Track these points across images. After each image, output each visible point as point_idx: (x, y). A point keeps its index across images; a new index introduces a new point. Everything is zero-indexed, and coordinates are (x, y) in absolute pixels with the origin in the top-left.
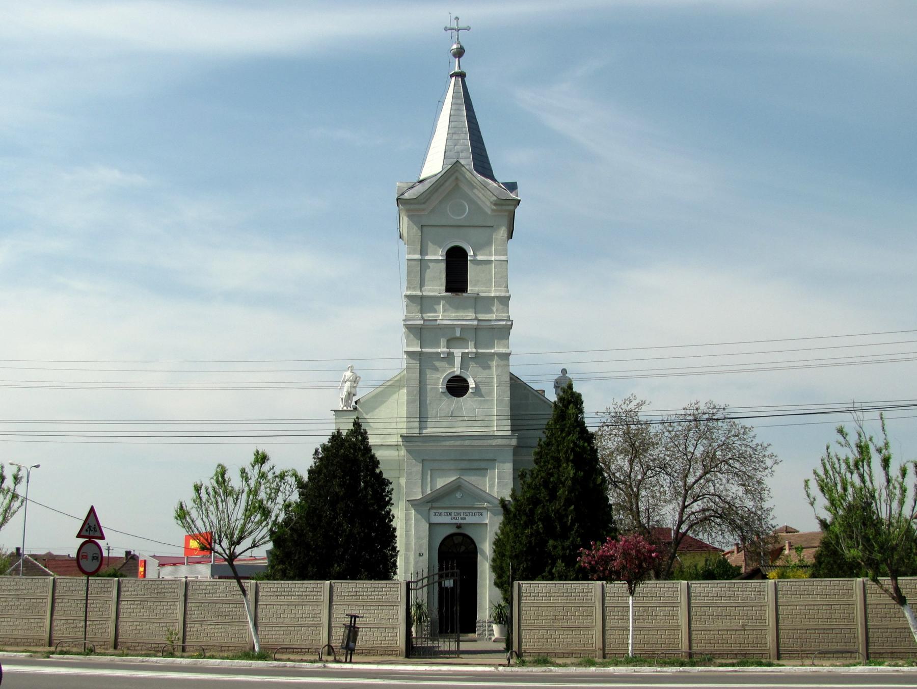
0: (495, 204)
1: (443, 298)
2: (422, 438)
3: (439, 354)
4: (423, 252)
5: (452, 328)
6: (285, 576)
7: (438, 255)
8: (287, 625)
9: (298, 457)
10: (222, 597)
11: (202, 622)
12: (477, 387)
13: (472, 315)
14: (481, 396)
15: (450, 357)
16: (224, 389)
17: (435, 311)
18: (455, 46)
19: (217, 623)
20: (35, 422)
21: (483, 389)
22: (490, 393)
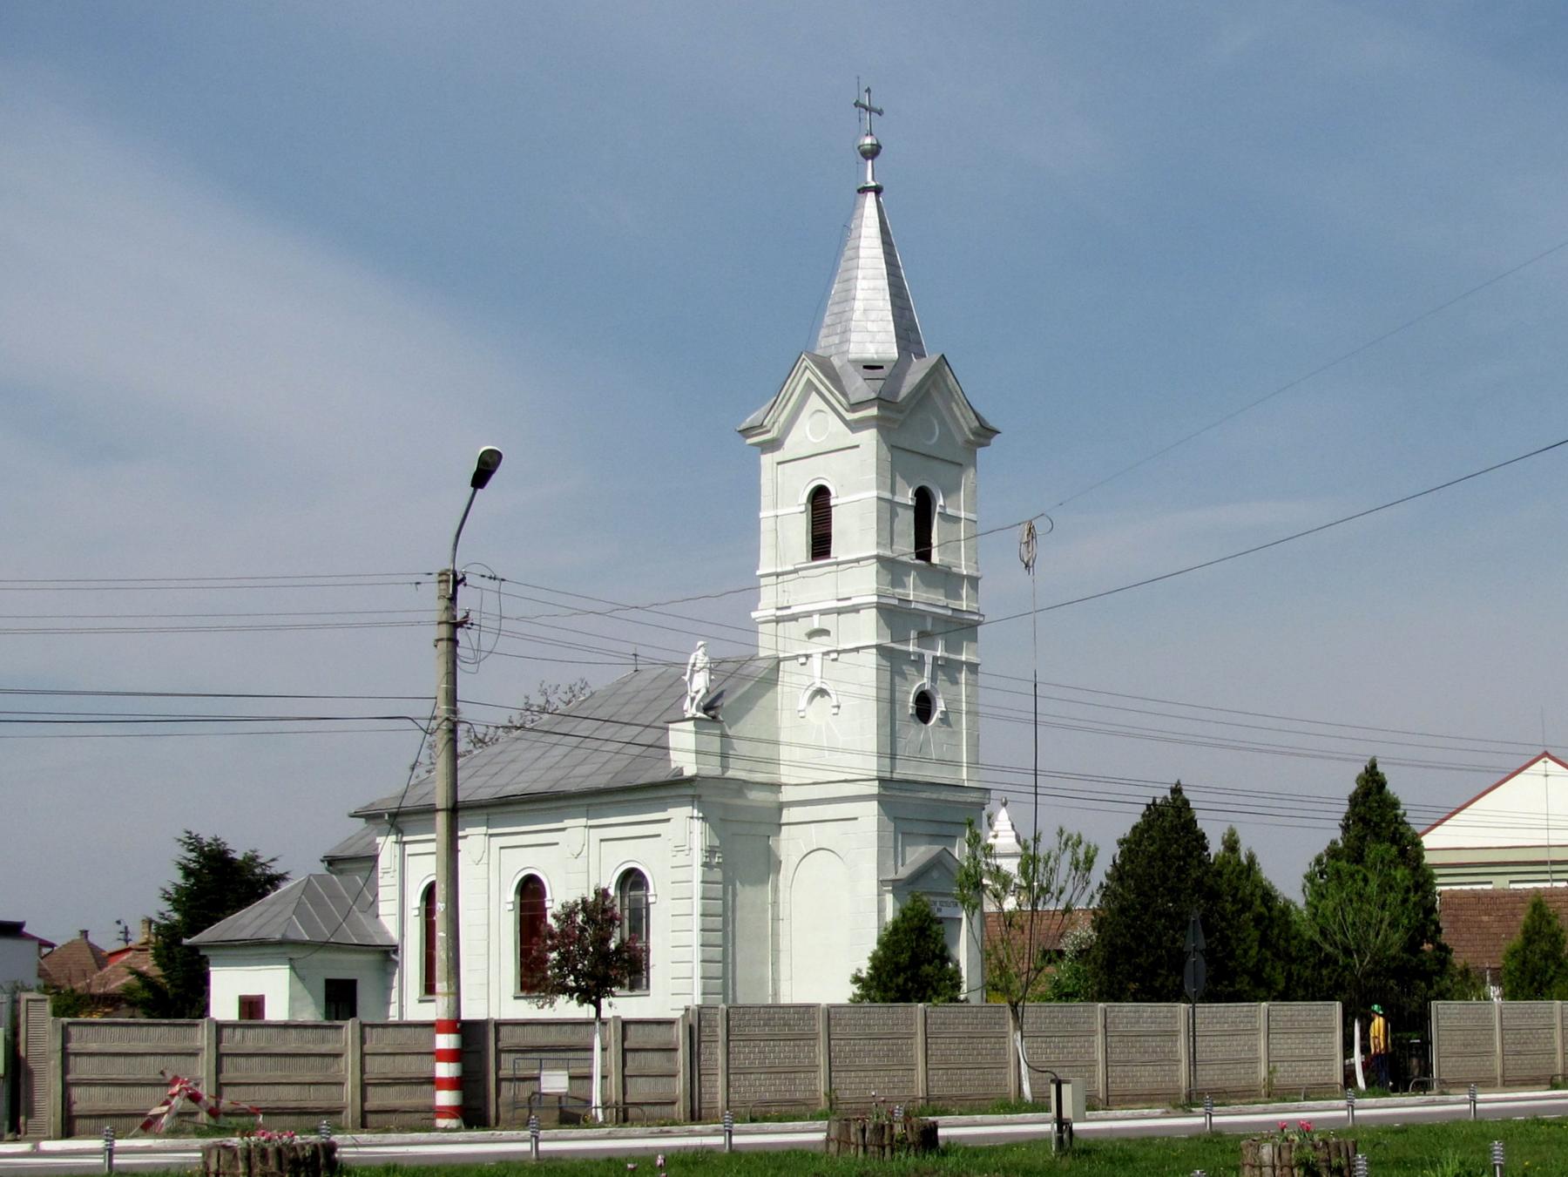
0: (974, 433)
1: (915, 567)
2: (891, 780)
3: (909, 653)
4: (893, 492)
5: (922, 615)
6: (1113, 993)
7: (908, 497)
8: (1223, 1062)
9: (1108, 830)
10: (1144, 1028)
11: (1126, 1063)
12: (945, 713)
13: (943, 601)
14: (949, 725)
15: (919, 662)
16: (1234, 748)
17: (904, 586)
18: (868, 141)
19: (1144, 1064)
20: (1003, 769)
21: (952, 717)
22: (959, 721)
